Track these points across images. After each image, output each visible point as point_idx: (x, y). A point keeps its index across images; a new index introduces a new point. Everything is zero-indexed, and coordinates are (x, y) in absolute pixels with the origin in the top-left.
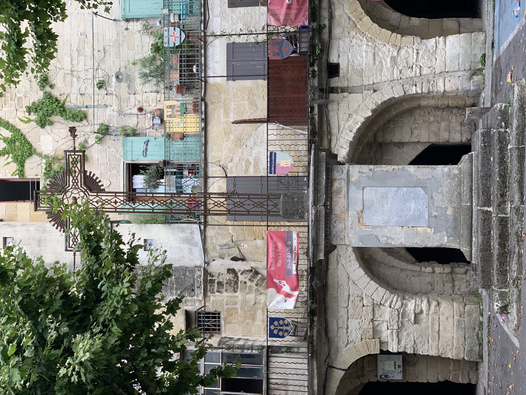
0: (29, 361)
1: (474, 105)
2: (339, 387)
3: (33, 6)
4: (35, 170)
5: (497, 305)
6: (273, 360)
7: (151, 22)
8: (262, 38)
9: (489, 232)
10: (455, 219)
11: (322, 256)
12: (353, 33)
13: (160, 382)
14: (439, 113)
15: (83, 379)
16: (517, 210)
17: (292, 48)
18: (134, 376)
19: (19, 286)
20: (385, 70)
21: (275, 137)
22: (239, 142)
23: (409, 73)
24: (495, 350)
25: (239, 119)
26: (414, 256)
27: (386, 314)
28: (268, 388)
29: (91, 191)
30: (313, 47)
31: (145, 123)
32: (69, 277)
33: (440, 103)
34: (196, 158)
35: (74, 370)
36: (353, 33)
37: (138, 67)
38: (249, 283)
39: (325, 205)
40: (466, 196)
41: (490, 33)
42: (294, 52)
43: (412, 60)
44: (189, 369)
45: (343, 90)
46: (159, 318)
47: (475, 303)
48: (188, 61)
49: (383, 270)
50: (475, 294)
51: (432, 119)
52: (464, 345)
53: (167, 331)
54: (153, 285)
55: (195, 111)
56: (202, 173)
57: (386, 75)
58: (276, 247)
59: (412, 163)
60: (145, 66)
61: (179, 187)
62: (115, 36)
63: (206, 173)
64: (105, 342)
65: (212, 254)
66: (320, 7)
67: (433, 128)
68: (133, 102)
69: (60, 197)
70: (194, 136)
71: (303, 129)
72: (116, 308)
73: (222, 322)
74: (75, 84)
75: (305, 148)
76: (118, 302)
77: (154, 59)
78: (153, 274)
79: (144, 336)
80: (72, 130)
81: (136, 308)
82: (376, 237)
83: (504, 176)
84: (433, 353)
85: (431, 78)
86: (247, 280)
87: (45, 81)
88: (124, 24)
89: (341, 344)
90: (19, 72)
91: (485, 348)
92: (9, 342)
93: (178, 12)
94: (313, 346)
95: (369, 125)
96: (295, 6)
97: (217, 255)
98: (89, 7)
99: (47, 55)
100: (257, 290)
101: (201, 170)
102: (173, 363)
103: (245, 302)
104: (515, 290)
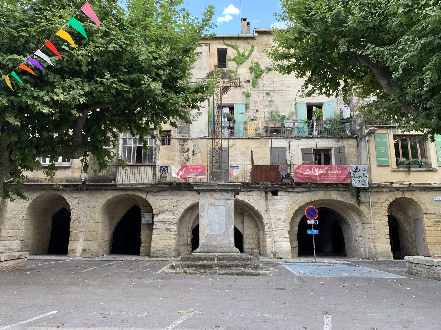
0: (150, 62)
1: (260, 254)
2: (138, 196)
3: (302, 64)
4: (231, 65)
5: (174, 264)
6: (150, 168)
7: (295, 115)
8: (288, 163)
9: (206, 260)
10: (211, 246)
11: (195, 188)
12: (291, 202)
13: (141, 119)
14: (257, 239)
15: (143, 86)
16: (216, 272)
17: (284, 175)
18: (143, 108)
19: (182, 58)
20: (275, 215)
21: (245, 168)
22: (243, 153)
23: (274, 226)
24: (155, 263)
25: (253, 153)
26: (195, 228)
27: (170, 216)
28: (138, 166)
29: (223, 89)
30: (285, 184)
31: (252, 113)
32: (186, 80)
33: (261, 239)
34: (236, 135)
35: (147, 82)
36: (291, 202)
37: (276, 110)
38: (183, 157)
39: (217, 189)
40: (221, 250)
41: (291, 261)
42: (282, 176)
43: (280, 227)
44: (146, 131)
45: (266, 197)
46: (168, 119)
47: (175, 255)
48: (278, 131)
49: (189, 215)
50: (179, 255)
51: (254, 236)
52: (157, 250)
53: (163, 122)
54: (182, 116)
55: (257, 134)
56: (230, 137)
57: (273, 216)
58: (199, 169)
59: (235, 228)
60: (276, 112)
61: (224, 127)
62: (289, 100)
63: (230, 139)
64: (158, 95)
65: (196, 141)
66: (302, 187)
67: (250, 236)
68: (260, 108)
69: (220, 76)
70: (246, 134)
71: (249, 180)
72: (172, 100)
73: (166, 146)
74: (268, 83)
75: (241, 181)
76: (175, 101)
77: (279, 116)
78: (187, 116)
79: (161, 112)
80: (248, 81)
81: (173, 108)
82: (203, 212)
83: (230, 266)
84: (153, 237)
85: (272, 235)
86: (184, 156)
87: (269, 70)
88: (294, 103)
89: (157, 197)
90: (273, 58)
91: (156, 259)
92: (158, 54)
93: (299, 126)
94: (156, 185)
95: (251, 208)
96: (302, 177)
97: (195, 143)
98: (302, 88)
99: (281, 70)
100: (180, 161)
101: (231, 136)
102: (148, 125)
103: (175, 156)
104: (181, 272)
